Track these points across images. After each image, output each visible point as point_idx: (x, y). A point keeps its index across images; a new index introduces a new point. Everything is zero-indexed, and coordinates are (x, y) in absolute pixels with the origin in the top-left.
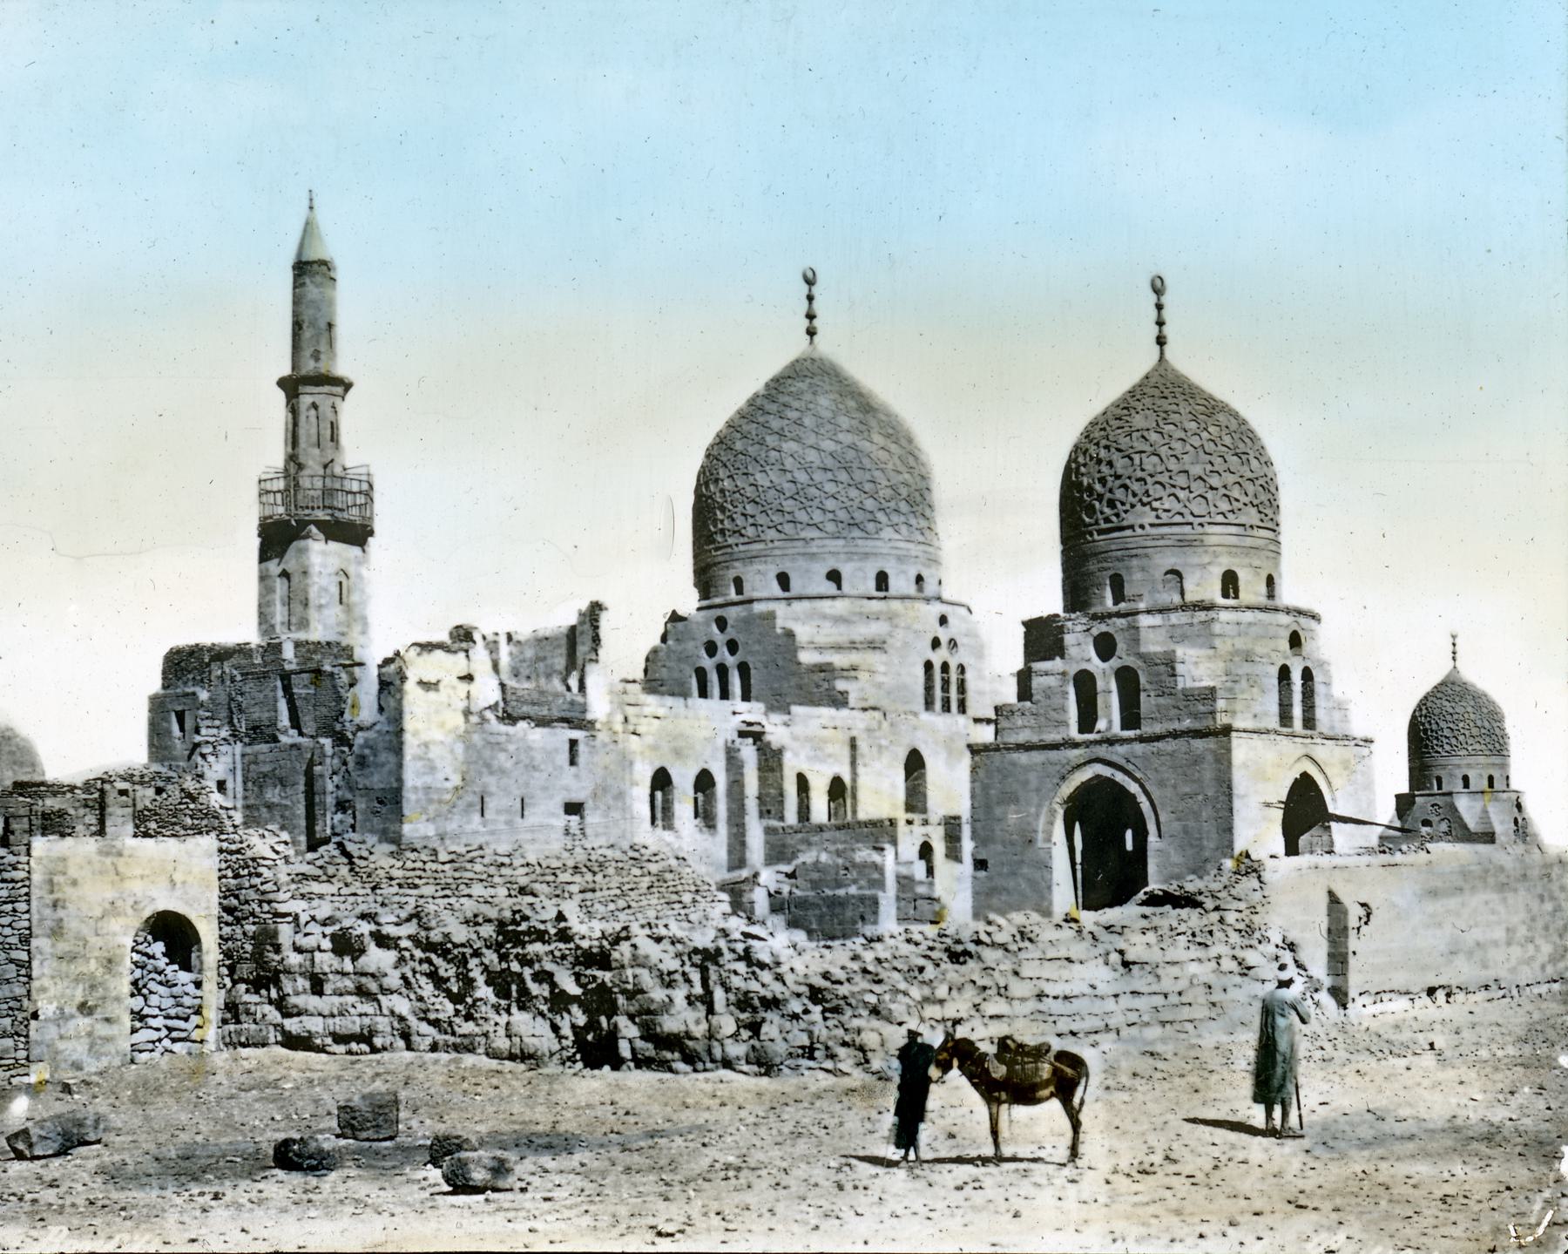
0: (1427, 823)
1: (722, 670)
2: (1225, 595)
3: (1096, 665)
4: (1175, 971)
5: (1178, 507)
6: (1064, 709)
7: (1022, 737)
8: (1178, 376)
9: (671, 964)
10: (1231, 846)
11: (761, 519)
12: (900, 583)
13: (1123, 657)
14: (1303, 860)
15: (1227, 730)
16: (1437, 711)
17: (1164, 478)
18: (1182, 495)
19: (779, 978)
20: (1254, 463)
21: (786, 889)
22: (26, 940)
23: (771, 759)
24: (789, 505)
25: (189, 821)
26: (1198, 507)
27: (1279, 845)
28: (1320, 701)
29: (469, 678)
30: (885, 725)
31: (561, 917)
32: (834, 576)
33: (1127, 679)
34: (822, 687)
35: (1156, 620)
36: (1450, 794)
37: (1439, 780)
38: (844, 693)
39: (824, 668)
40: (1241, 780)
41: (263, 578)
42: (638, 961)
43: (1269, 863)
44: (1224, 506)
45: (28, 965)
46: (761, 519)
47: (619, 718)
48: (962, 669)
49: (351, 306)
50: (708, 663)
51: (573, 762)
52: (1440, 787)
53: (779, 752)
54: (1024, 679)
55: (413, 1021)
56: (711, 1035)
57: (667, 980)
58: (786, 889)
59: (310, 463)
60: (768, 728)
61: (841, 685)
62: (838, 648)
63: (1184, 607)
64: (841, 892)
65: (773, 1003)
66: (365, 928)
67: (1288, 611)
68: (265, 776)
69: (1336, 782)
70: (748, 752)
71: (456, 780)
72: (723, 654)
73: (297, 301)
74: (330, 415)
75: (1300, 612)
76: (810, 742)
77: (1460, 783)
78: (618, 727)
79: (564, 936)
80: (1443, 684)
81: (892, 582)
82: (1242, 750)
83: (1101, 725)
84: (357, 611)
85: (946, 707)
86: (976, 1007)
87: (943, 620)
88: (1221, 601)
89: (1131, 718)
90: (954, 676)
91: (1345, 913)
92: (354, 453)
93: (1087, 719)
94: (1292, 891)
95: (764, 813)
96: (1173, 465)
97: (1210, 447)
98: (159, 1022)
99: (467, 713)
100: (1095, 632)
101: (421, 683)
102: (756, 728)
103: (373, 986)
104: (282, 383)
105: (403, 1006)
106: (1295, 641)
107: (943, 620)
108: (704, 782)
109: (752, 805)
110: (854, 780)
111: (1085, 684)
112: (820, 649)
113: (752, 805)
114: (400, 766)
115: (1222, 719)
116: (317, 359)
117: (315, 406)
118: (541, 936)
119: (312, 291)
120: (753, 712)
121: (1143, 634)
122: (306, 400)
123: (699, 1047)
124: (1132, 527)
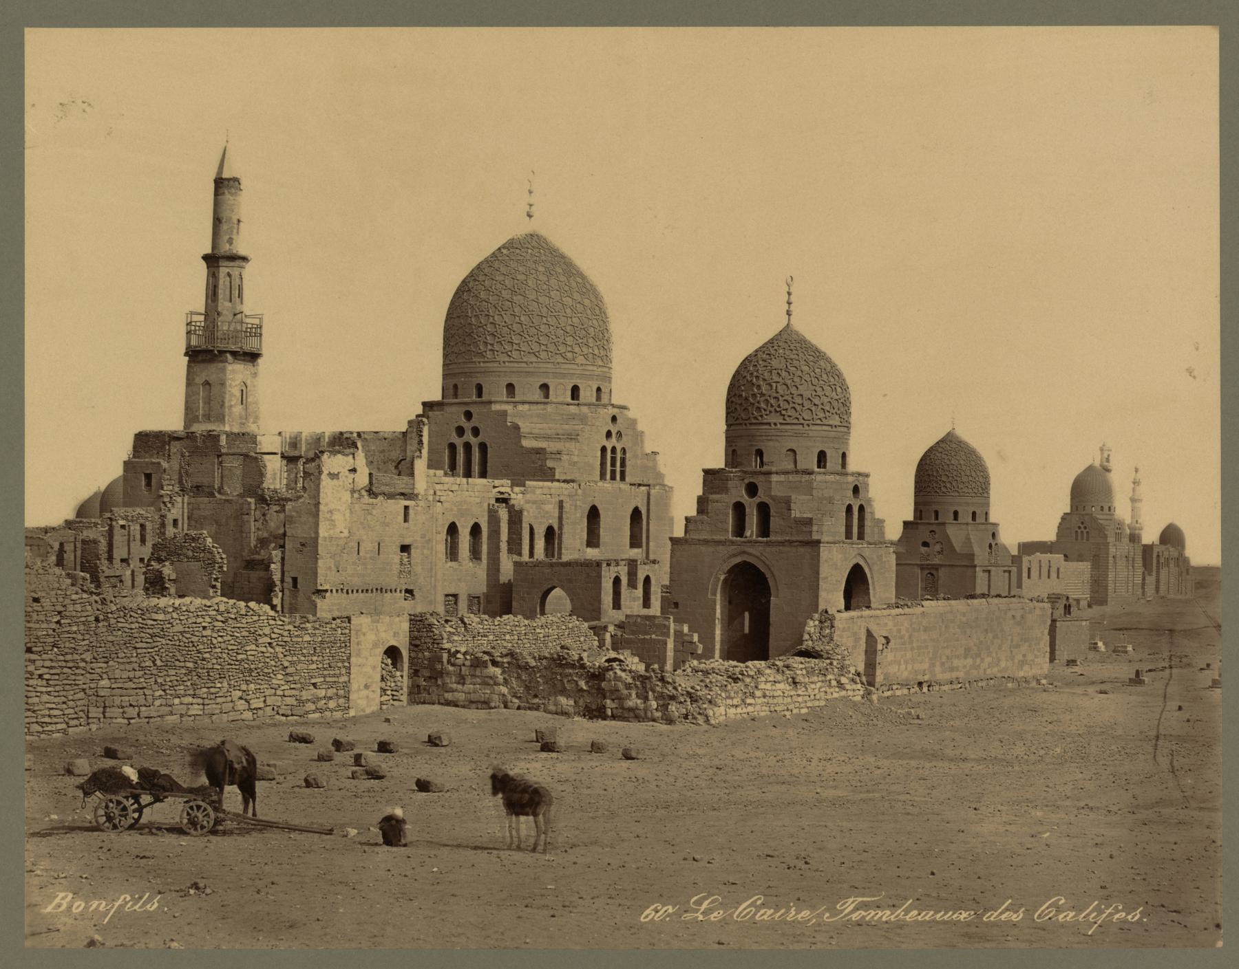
0: (925, 544)
1: (468, 447)
2: (819, 467)
3: (745, 499)
4: (813, 686)
5: (797, 415)
6: (726, 522)
7: (705, 536)
8: (797, 333)
9: (630, 680)
10: (817, 606)
11: (496, 347)
12: (587, 395)
13: (762, 497)
14: (852, 613)
15: (819, 542)
16: (938, 462)
17: (789, 398)
18: (798, 408)
19: (675, 688)
20: (839, 390)
21: (619, 634)
22: (349, 658)
23: (516, 518)
24: (516, 339)
25: (190, 553)
26: (807, 415)
27: (841, 603)
28: (868, 523)
29: (354, 470)
30: (580, 492)
31: (581, 659)
32: (545, 387)
33: (764, 510)
34: (535, 466)
35: (782, 478)
36: (944, 524)
37: (937, 513)
38: (552, 469)
39: (540, 452)
40: (824, 570)
41: (189, 382)
42: (617, 678)
43: (838, 616)
44: (821, 415)
45: (349, 668)
46: (496, 347)
47: (432, 492)
48: (624, 450)
49: (245, 205)
50: (459, 442)
51: (406, 520)
52: (937, 518)
53: (521, 512)
54: (702, 501)
55: (509, 697)
56: (646, 710)
57: (628, 686)
58: (619, 634)
59: (225, 312)
60: (513, 496)
61: (550, 464)
62: (547, 438)
63: (797, 472)
64: (647, 637)
65: (673, 698)
66: (486, 658)
67: (853, 474)
68: (205, 518)
69: (875, 576)
70: (503, 514)
71: (346, 533)
72: (469, 437)
73: (217, 204)
74: (238, 281)
75: (860, 474)
76: (537, 502)
77: (952, 516)
78: (431, 498)
79: (583, 666)
80: (942, 441)
81: (582, 393)
82: (824, 552)
83: (748, 533)
84: (251, 408)
85: (613, 478)
86: (743, 701)
87: (614, 419)
88: (817, 470)
89: (764, 530)
90: (619, 455)
91: (876, 642)
92: (251, 305)
93: (740, 530)
94: (849, 628)
95: (510, 551)
96: (793, 390)
97: (815, 381)
98: (389, 692)
99: (353, 491)
100: (746, 481)
101: (330, 474)
102: (506, 496)
103: (491, 682)
104: (206, 258)
105: (504, 690)
106: (856, 490)
107: (614, 419)
108: (476, 530)
109: (504, 546)
110: (560, 528)
111: (739, 508)
112: (536, 438)
113: (504, 546)
114: (317, 524)
115: (815, 537)
116: (231, 244)
117: (229, 275)
118: (573, 666)
119: (227, 197)
120: (504, 485)
121: (773, 485)
122: (223, 271)
123: (642, 714)
124: (769, 424)
